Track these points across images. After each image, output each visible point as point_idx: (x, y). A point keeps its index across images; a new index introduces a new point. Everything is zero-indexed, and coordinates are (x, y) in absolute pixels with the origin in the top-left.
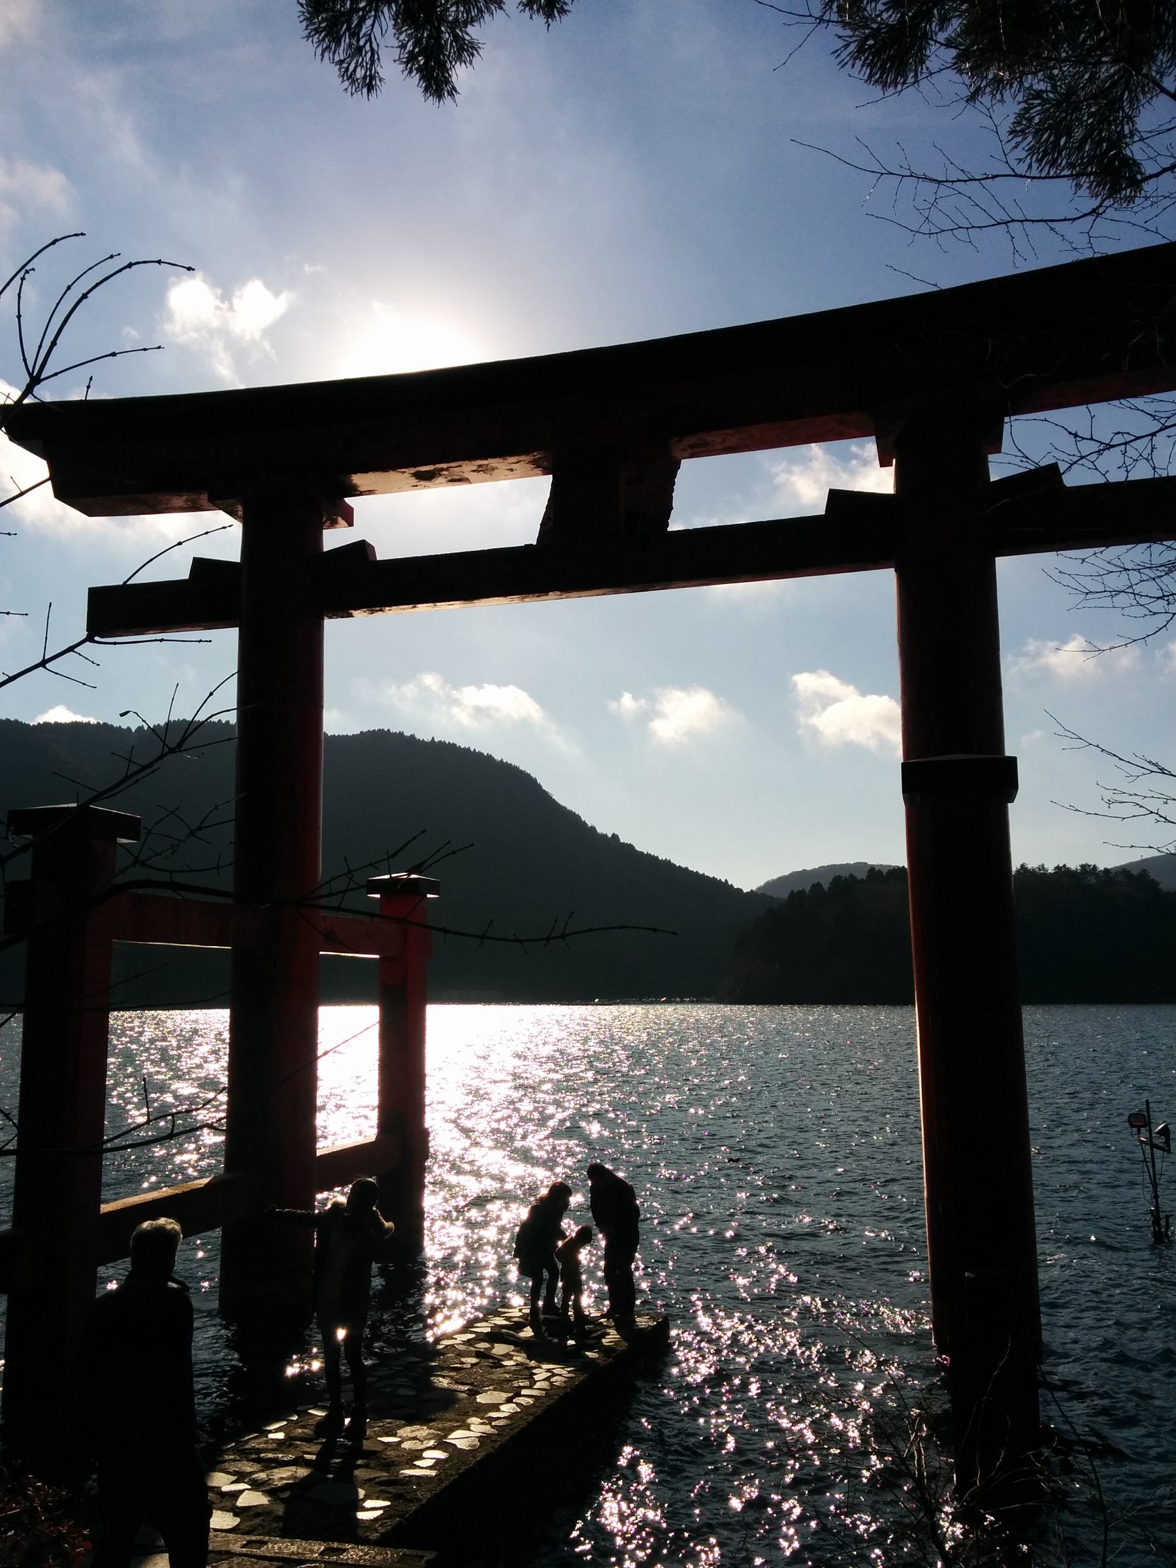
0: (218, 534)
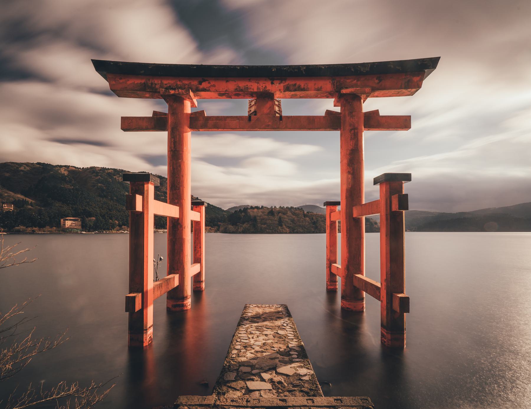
0: (328, 105)
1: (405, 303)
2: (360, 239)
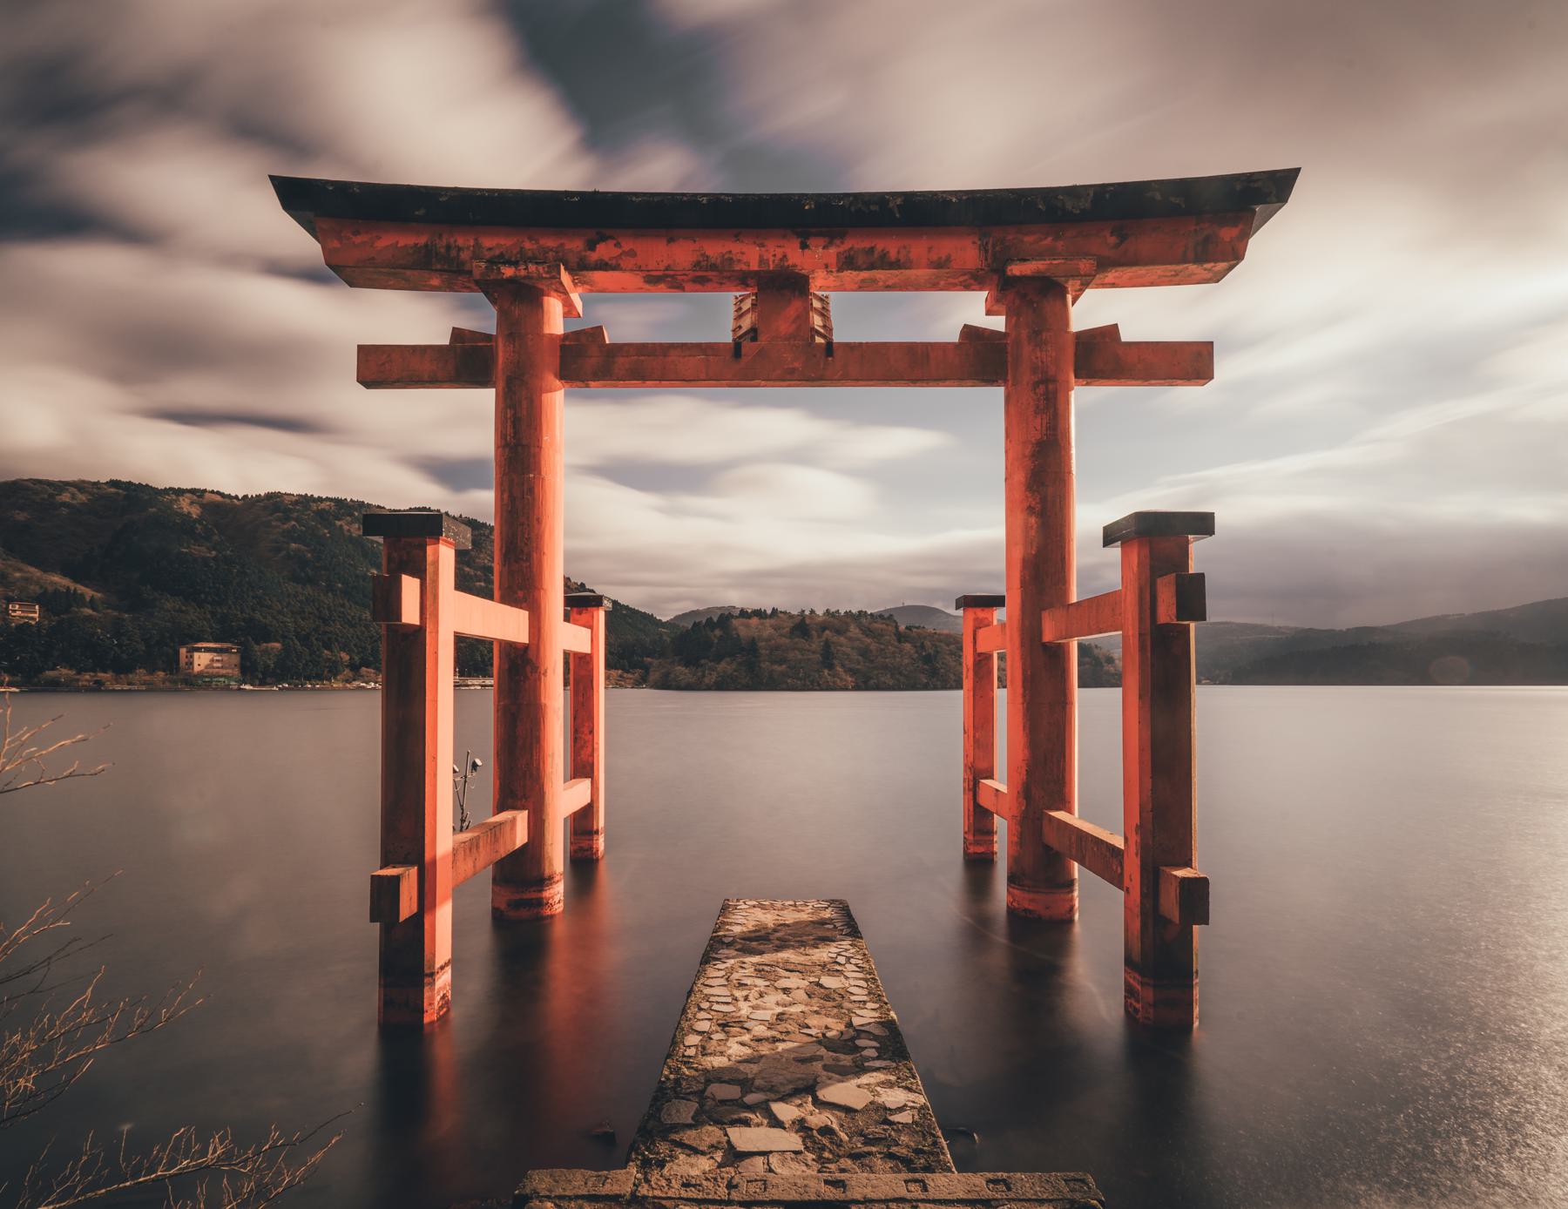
1: (1196, 896)
2: (1064, 708)
